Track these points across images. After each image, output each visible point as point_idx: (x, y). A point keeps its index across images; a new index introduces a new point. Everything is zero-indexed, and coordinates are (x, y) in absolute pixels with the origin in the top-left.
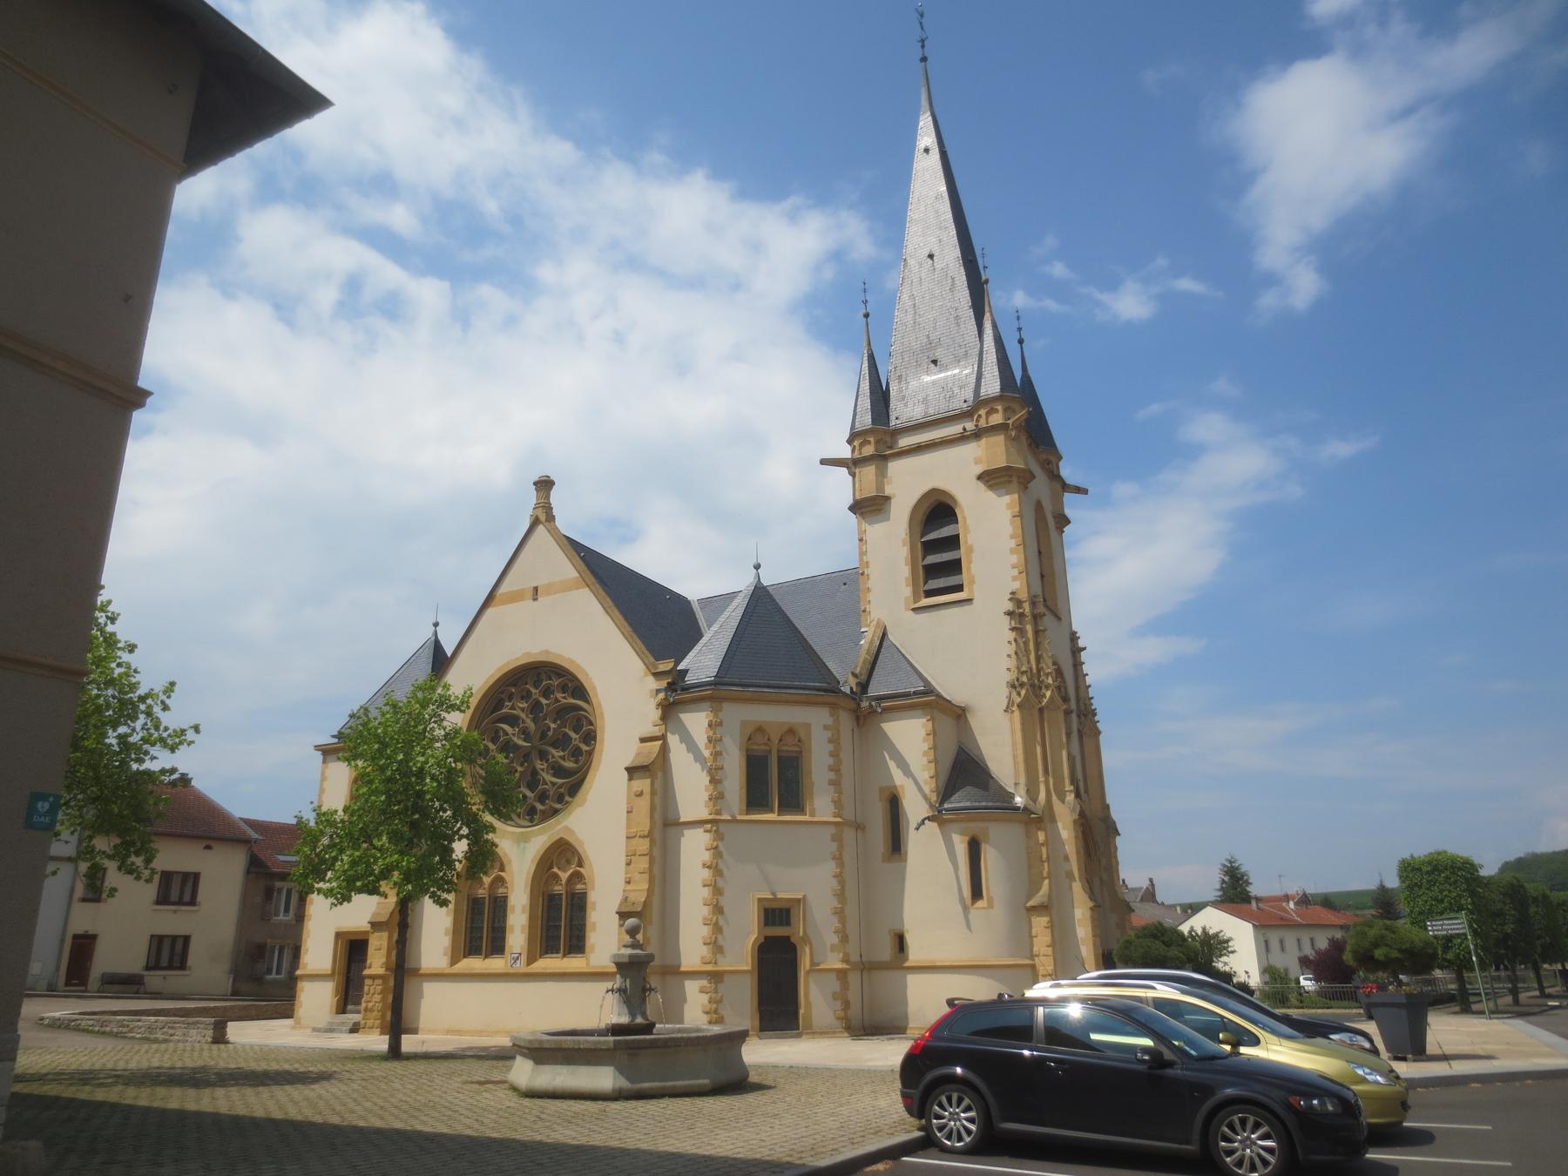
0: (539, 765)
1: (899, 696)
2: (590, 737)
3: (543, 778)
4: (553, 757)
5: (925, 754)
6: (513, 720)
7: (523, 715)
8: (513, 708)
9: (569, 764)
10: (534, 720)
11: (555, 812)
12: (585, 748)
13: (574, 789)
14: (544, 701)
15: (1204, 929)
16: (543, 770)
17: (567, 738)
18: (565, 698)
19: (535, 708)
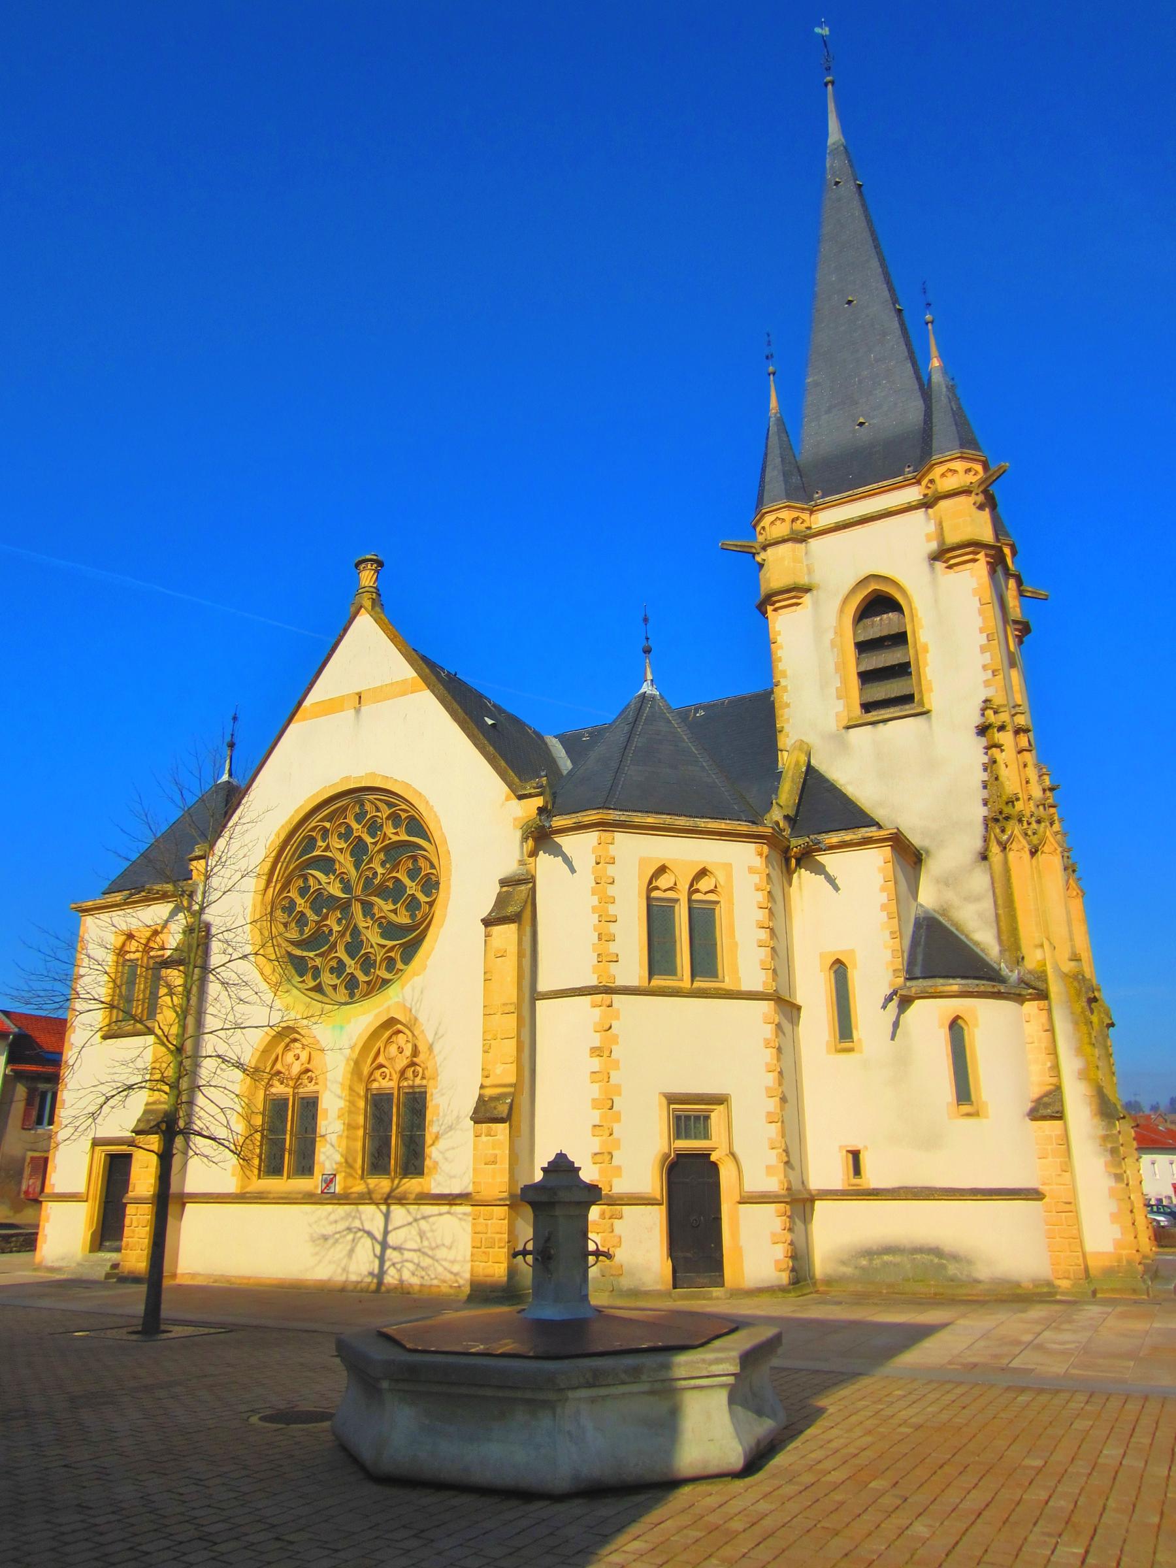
0: (361, 922)
1: (971, 459)
2: (431, 885)
3: (367, 939)
4: (381, 910)
5: (883, 907)
6: (326, 864)
7: (340, 857)
8: (327, 848)
9: (403, 919)
10: (357, 866)
11: (385, 982)
12: (422, 898)
13: (410, 950)
14: (369, 840)
15: (1032, 1102)
16: (367, 928)
17: (399, 885)
18: (396, 834)
19: (359, 850)
